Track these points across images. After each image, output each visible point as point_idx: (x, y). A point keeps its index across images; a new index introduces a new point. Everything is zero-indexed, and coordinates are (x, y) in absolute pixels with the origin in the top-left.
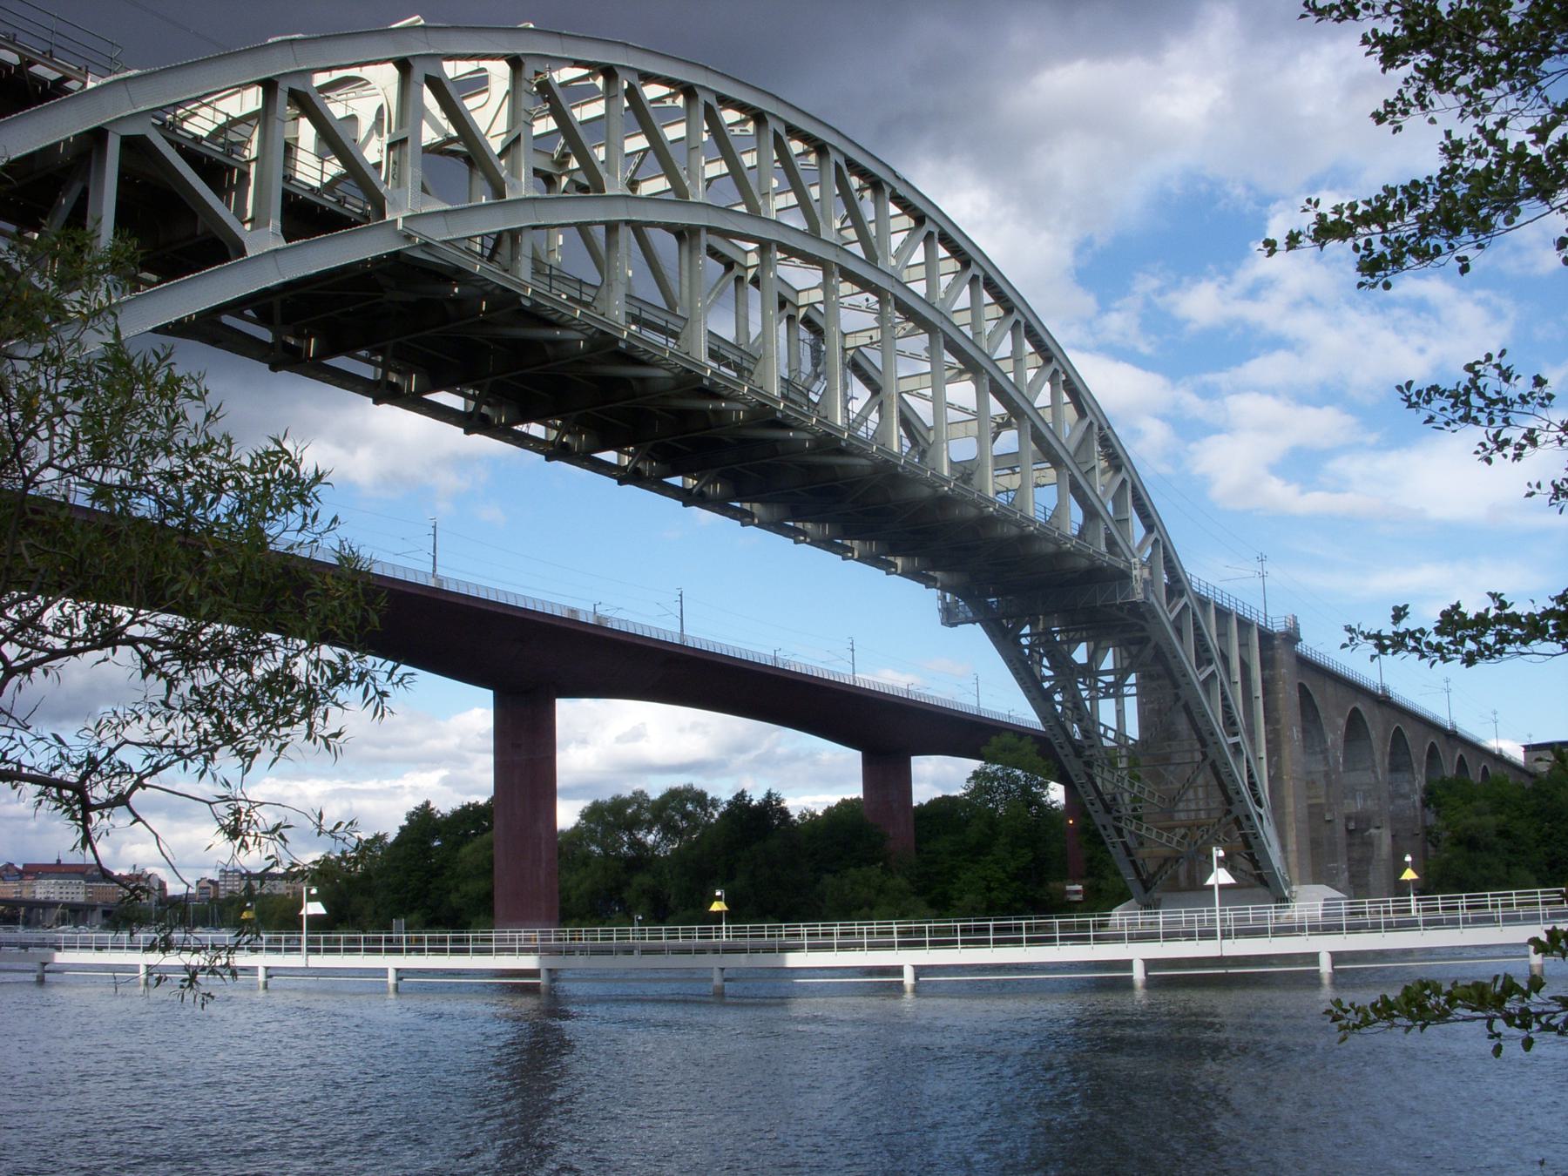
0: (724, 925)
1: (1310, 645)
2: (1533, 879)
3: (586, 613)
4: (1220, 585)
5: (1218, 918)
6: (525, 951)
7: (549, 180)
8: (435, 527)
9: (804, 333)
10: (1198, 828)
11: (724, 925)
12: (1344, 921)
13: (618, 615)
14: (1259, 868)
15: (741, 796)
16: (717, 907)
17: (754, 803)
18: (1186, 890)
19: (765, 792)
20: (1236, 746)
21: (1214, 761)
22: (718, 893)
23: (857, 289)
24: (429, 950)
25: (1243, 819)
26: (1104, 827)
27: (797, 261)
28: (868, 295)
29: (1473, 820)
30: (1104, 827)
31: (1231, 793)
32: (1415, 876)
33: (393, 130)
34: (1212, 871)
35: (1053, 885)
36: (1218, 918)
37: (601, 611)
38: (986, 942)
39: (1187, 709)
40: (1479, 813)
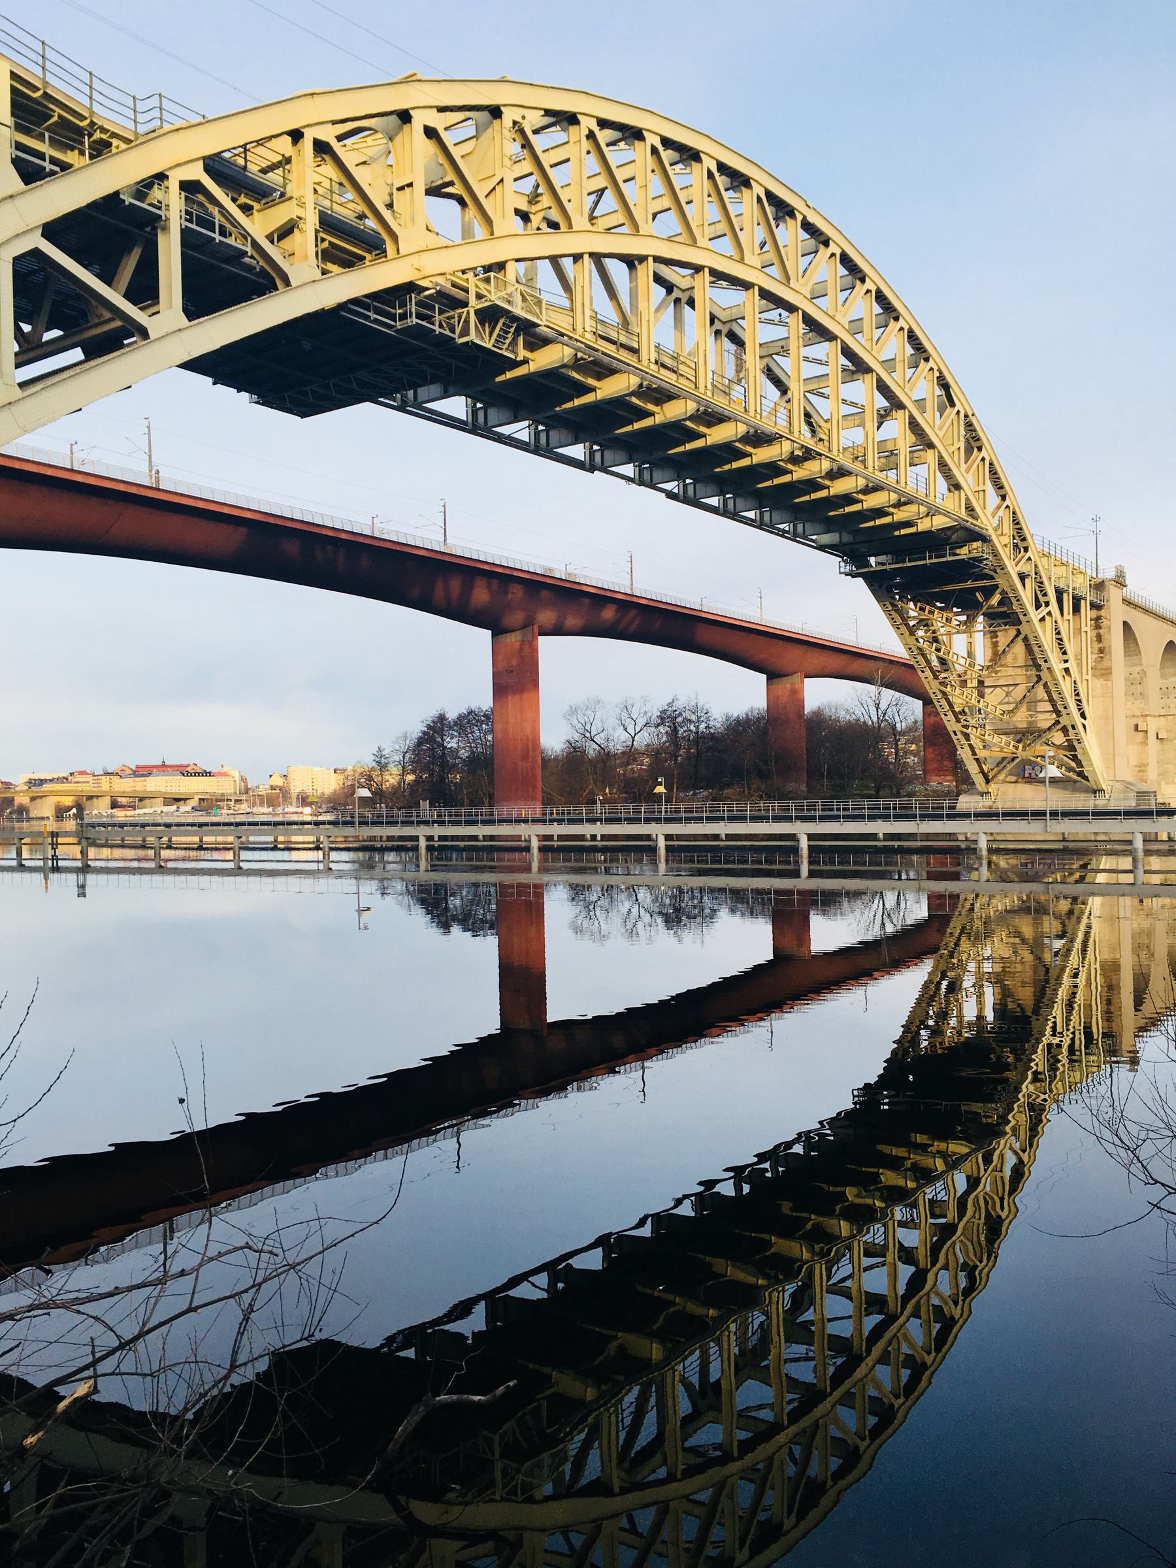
1: (1133, 590)
3: (560, 571)
4: (1141, 594)
5: (663, 810)
7: (525, 217)
8: (444, 506)
9: (727, 344)
12: (683, 815)
13: (584, 572)
14: (1082, 767)
20: (1067, 670)
21: (1046, 682)
22: (660, 780)
23: (772, 306)
24: (449, 822)
25: (1070, 728)
26: (955, 733)
27: (724, 283)
28: (780, 311)
30: (955, 733)
31: (1060, 708)
36: (663, 810)
37: (570, 569)
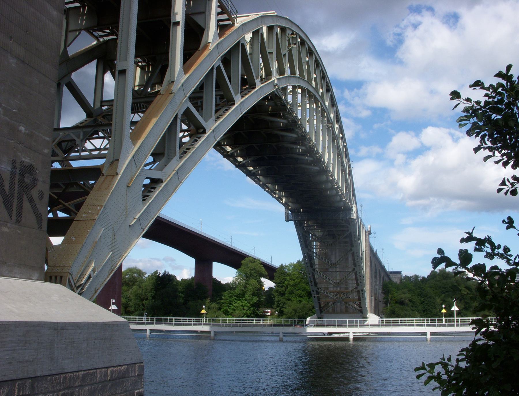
0: (455, 318)
2: (419, 315)
6: (204, 325)
10: (341, 293)
11: (455, 318)
15: (156, 272)
16: (203, 311)
17: (161, 275)
18: (331, 313)
19: (164, 272)
25: (361, 291)
26: (313, 291)
29: (403, 296)
32: (446, 312)
33: (274, 12)
34: (110, 306)
35: (261, 310)
38: (390, 326)
39: (353, 254)
40: (404, 293)
